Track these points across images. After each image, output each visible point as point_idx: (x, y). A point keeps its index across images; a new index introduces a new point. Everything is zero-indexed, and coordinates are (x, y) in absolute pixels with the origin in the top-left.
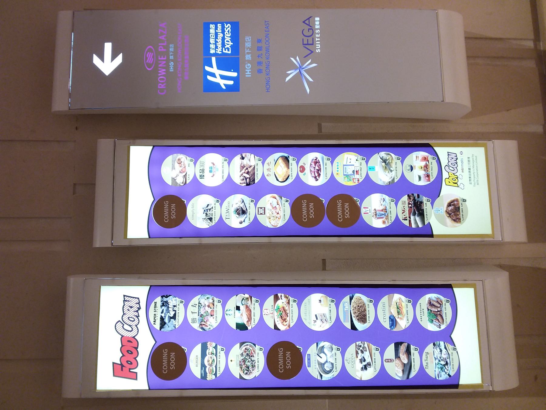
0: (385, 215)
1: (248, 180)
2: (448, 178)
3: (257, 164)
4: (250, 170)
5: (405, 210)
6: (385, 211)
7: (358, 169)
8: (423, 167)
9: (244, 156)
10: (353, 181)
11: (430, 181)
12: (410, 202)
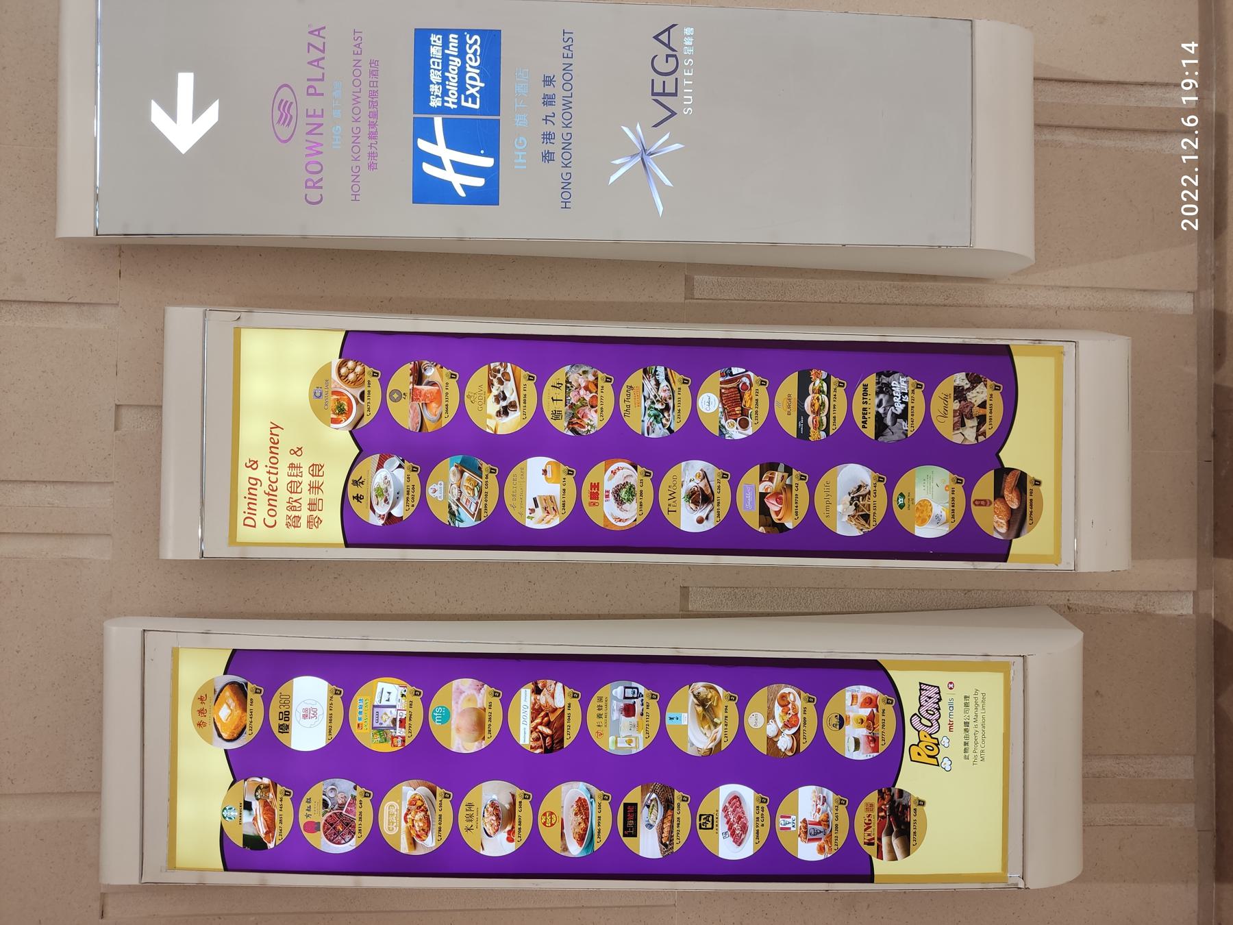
1: (548, 740)
2: (918, 745)
3: (570, 704)
4: (553, 717)
7: (404, 714)
8: (865, 719)
9: (540, 685)
12: (883, 807)
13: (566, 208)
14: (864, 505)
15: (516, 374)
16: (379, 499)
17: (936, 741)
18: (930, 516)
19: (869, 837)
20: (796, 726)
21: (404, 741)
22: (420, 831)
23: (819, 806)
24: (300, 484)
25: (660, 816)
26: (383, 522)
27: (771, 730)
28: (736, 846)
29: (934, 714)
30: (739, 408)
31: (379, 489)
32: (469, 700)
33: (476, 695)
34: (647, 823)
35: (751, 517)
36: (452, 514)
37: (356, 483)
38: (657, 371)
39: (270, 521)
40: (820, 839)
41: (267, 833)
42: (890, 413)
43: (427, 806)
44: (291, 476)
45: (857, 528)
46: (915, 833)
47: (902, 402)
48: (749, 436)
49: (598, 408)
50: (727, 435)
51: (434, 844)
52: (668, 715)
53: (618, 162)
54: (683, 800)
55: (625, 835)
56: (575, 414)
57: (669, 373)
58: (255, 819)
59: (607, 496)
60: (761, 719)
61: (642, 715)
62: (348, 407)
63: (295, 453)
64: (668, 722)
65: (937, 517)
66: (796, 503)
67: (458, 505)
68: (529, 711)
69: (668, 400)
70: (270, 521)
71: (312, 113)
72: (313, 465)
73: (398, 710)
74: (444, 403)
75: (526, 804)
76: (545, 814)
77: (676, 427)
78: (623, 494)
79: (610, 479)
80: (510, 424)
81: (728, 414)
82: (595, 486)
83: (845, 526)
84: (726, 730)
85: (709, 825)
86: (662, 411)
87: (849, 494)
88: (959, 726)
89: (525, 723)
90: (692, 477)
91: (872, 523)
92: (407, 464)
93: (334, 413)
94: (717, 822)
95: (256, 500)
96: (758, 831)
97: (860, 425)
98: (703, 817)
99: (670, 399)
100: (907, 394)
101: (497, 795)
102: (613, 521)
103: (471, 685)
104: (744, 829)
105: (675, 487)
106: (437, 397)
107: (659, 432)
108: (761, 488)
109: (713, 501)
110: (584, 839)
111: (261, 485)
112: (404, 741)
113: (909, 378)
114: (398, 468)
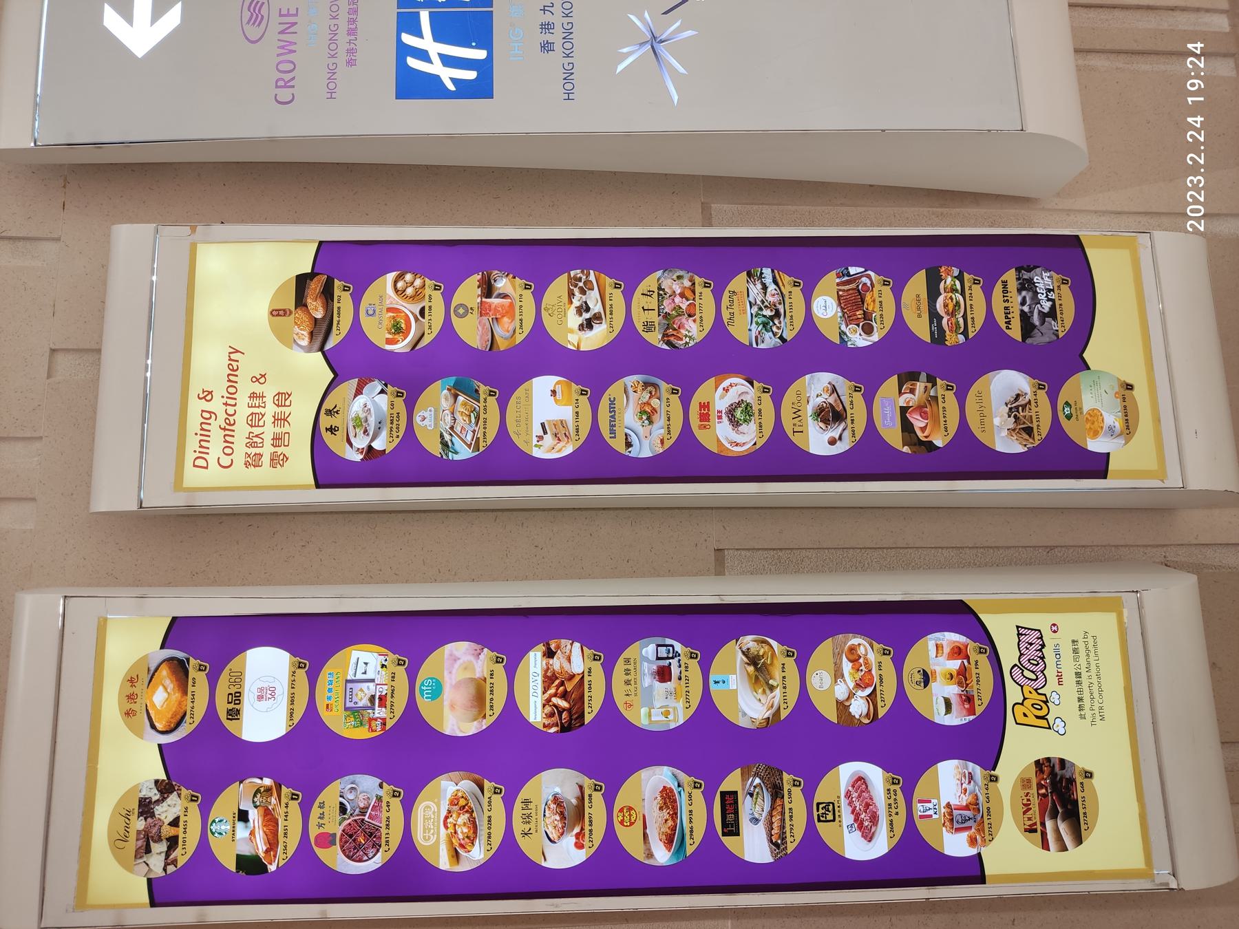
0: (975, 822)
1: (564, 715)
2: (1022, 704)
3: (590, 669)
5: (1030, 804)
6: (974, 809)
7: (385, 690)
8: (955, 674)
9: (553, 647)
10: (370, 725)
11: (975, 714)
12: (1043, 782)
13: (569, 99)
14: (1025, 417)
15: (601, 281)
16: (358, 430)
17: (1043, 698)
18: (1102, 428)
19: (1030, 822)
20: (871, 686)
21: (384, 724)
22: (463, 839)
23: (964, 786)
24: (263, 416)
25: (767, 807)
26: (362, 457)
27: (841, 692)
28: (866, 842)
29: (1038, 664)
30: (861, 312)
31: (357, 418)
32: (465, 669)
33: (475, 662)
34: (752, 816)
35: (893, 436)
36: (445, 445)
37: (329, 412)
38: (763, 273)
39: (226, 461)
40: (970, 828)
41: (267, 852)
42: (1036, 311)
43: (472, 806)
44: (252, 407)
45: (1020, 443)
46: (1085, 813)
47: (1049, 300)
48: (875, 343)
49: (697, 317)
50: (849, 343)
51: (482, 856)
52: (712, 678)
53: (625, 50)
54: (595, 790)
55: (724, 834)
56: (669, 323)
57: (777, 275)
58: (252, 833)
59: (720, 417)
60: (827, 678)
61: (680, 679)
62: (406, 324)
63: (258, 380)
64: (712, 686)
65: (1111, 429)
66: (944, 417)
67: (451, 435)
68: (540, 679)
69: (778, 305)
70: (226, 461)
71: (286, 12)
72: (279, 394)
73: (377, 684)
74: (518, 317)
75: (598, 798)
76: (621, 810)
77: (789, 336)
78: (738, 414)
79: (722, 397)
80: (597, 338)
81: (849, 319)
82: (705, 406)
83: (1006, 443)
84: (784, 695)
85: (830, 817)
86: (771, 318)
87: (1006, 404)
88: (1069, 678)
89: (535, 694)
90: (819, 392)
91: (1037, 437)
92: (390, 389)
93: (390, 333)
94: (839, 811)
95: (209, 436)
96: (891, 821)
97: (1003, 326)
98: (821, 806)
99: (780, 304)
100: (1053, 290)
101: (561, 787)
102: (728, 446)
103: (467, 650)
104: (874, 819)
105: (799, 404)
106: (510, 311)
107: (769, 341)
108: (902, 401)
109: (846, 418)
110: (672, 841)
111: (216, 420)
112: (384, 724)
113: (1052, 272)
114: (380, 393)
